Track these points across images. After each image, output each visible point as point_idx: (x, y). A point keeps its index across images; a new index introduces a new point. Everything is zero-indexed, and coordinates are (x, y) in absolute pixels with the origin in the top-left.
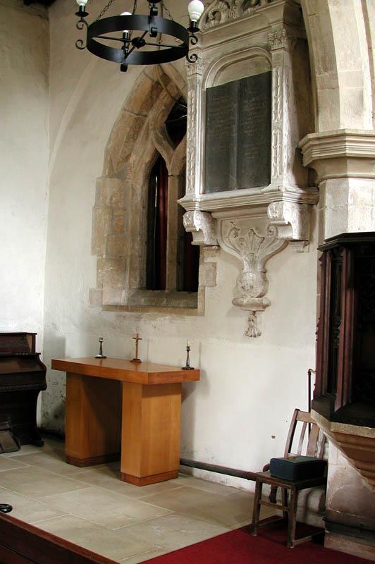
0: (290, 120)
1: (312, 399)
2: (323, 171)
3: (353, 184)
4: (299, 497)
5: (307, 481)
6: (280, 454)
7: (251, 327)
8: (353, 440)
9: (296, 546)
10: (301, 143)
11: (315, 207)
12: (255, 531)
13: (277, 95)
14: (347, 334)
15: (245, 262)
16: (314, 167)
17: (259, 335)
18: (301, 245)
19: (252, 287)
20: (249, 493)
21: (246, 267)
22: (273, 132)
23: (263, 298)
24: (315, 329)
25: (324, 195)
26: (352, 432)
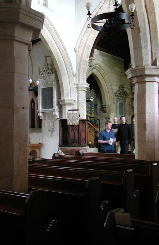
2: (63, 106)
20: (40, 154)
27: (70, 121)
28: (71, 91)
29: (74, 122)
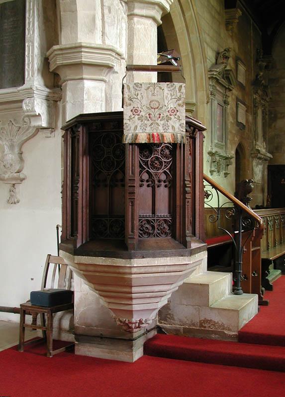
0: (39, 35)
1: (60, 242)
2: (65, 74)
3: (87, 84)
4: (54, 320)
5: (59, 306)
6: (38, 288)
7: (12, 196)
8: (92, 268)
9: (53, 356)
10: (48, 53)
11: (59, 103)
12: (22, 348)
13: (30, 16)
14: (84, 189)
15: (5, 146)
16: (57, 72)
17: (18, 202)
18: (48, 131)
19: (11, 165)
20: (16, 323)
21: (7, 150)
22: (27, 44)
23: (20, 173)
24: (60, 189)
25: (65, 91)
26: (90, 262)
27: (138, 123)
28: (106, 11)
29: (161, 130)
